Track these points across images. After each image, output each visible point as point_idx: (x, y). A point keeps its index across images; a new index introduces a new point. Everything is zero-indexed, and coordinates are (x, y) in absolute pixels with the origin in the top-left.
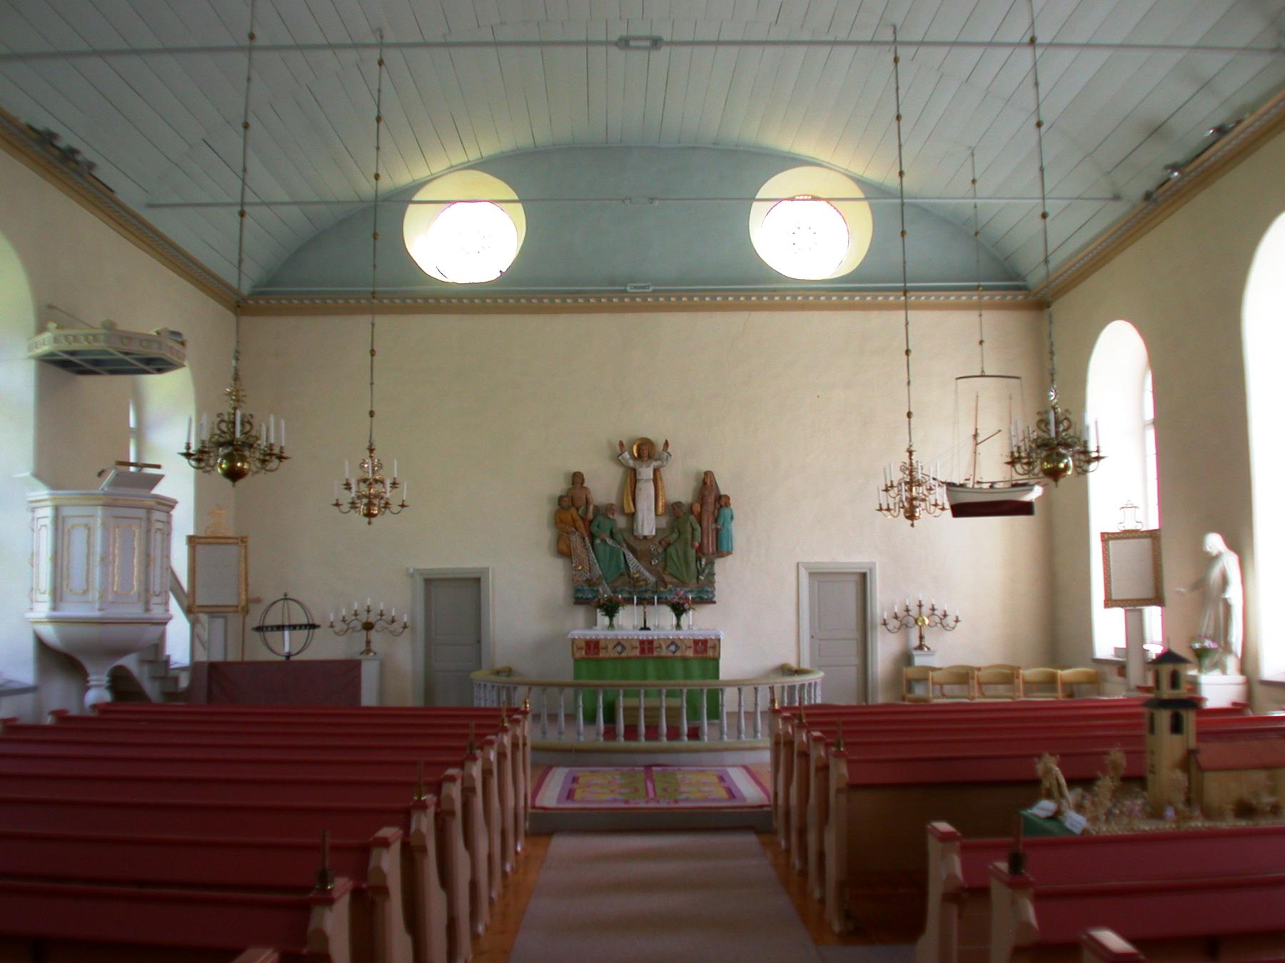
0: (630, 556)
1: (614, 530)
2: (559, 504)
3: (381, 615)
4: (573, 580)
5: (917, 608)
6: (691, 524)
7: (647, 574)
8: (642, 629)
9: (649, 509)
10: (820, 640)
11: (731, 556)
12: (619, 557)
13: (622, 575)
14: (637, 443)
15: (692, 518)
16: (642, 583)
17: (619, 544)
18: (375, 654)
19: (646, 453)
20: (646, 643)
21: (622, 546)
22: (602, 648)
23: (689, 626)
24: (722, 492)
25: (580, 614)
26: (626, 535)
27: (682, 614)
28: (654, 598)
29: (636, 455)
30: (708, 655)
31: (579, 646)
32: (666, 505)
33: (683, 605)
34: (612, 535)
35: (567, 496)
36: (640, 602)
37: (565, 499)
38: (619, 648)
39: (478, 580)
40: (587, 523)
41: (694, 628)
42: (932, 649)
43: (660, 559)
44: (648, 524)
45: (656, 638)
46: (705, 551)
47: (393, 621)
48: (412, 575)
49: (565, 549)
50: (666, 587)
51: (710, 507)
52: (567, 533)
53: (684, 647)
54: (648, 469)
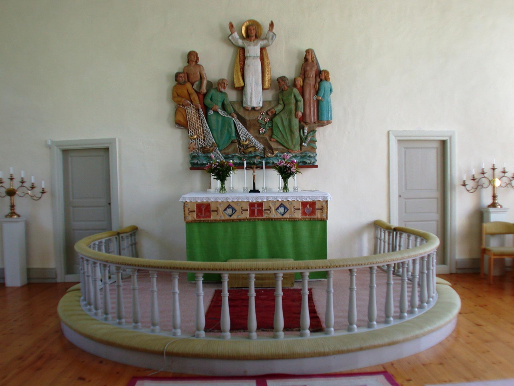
0: (240, 126)
1: (225, 103)
2: (176, 80)
3: (23, 182)
4: (189, 148)
5: (491, 171)
6: (295, 96)
7: (256, 141)
8: (251, 191)
9: (256, 83)
10: (405, 199)
11: (330, 125)
12: (231, 127)
13: (233, 142)
14: (246, 24)
15: (296, 91)
16: (251, 149)
17: (230, 115)
19: (254, 33)
20: (256, 206)
21: (233, 117)
22: (213, 211)
23: (294, 188)
24: (322, 69)
25: (197, 176)
26: (236, 107)
27: (289, 177)
28: (262, 163)
29: (244, 35)
30: (316, 217)
31: (191, 210)
32: (271, 81)
33: (290, 168)
34: (224, 108)
35: (183, 72)
36: (250, 166)
37: (181, 75)
38: (229, 211)
39: (107, 150)
40: (201, 97)
41: (299, 190)
42: (504, 207)
43: (267, 128)
44: (255, 97)
45: (265, 200)
46: (308, 120)
47: (33, 187)
48: (50, 147)
49: (182, 120)
50: (273, 153)
51: (311, 81)
52: (183, 106)
53: (293, 209)
54: (256, 47)
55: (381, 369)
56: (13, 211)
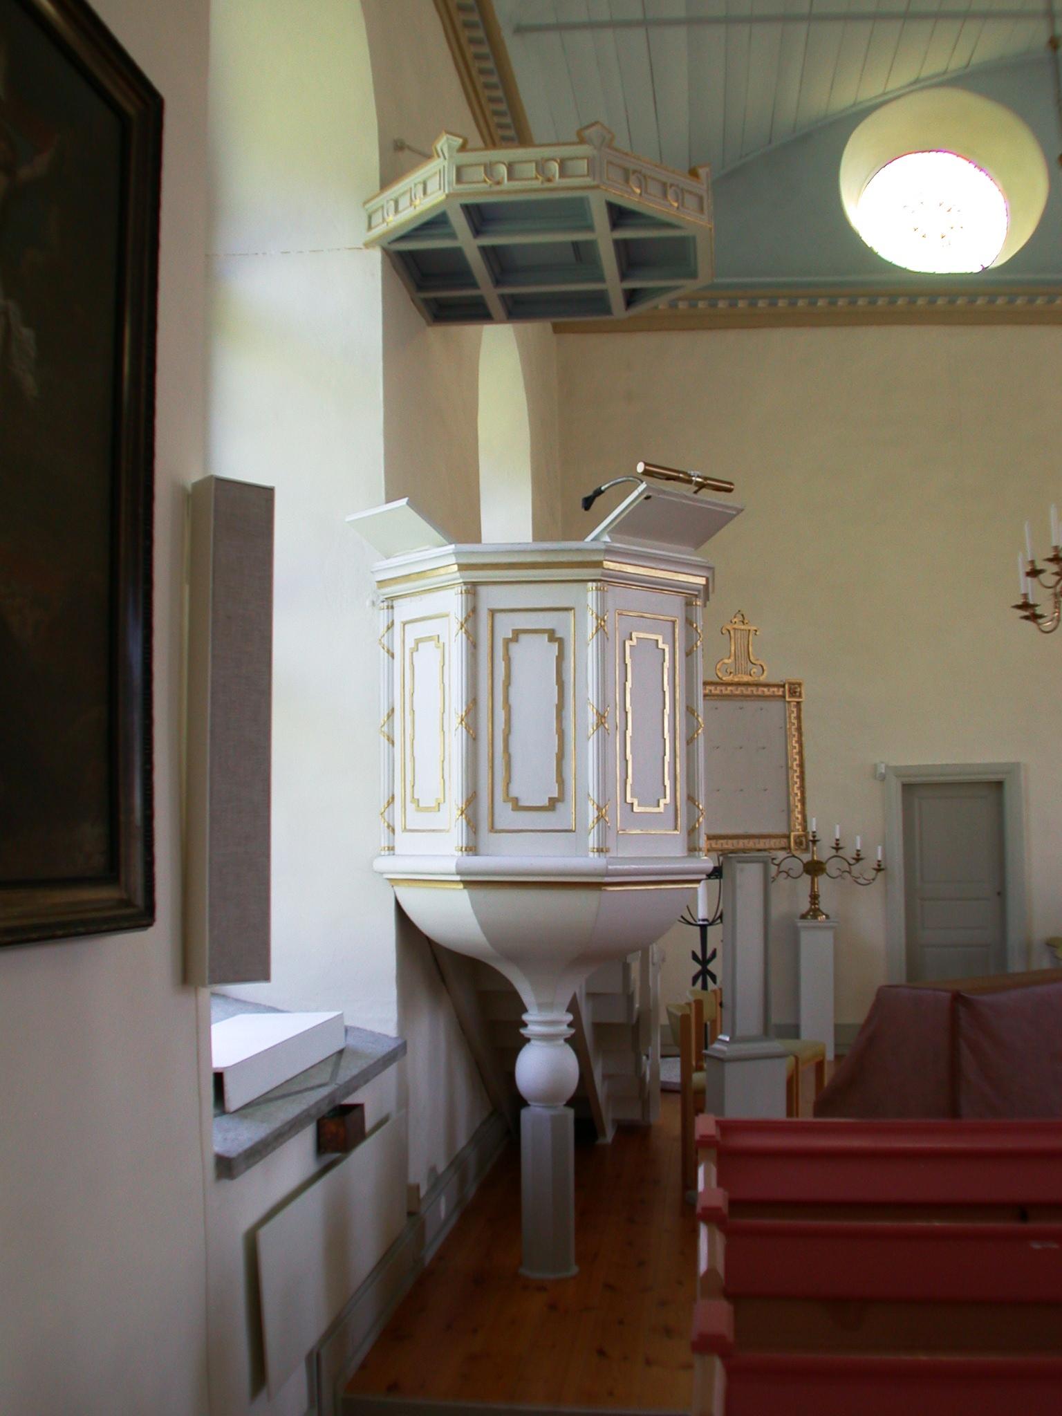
3: (837, 848)
18: (827, 917)
47: (858, 859)
48: (883, 778)
55: (402, 625)
56: (817, 906)
